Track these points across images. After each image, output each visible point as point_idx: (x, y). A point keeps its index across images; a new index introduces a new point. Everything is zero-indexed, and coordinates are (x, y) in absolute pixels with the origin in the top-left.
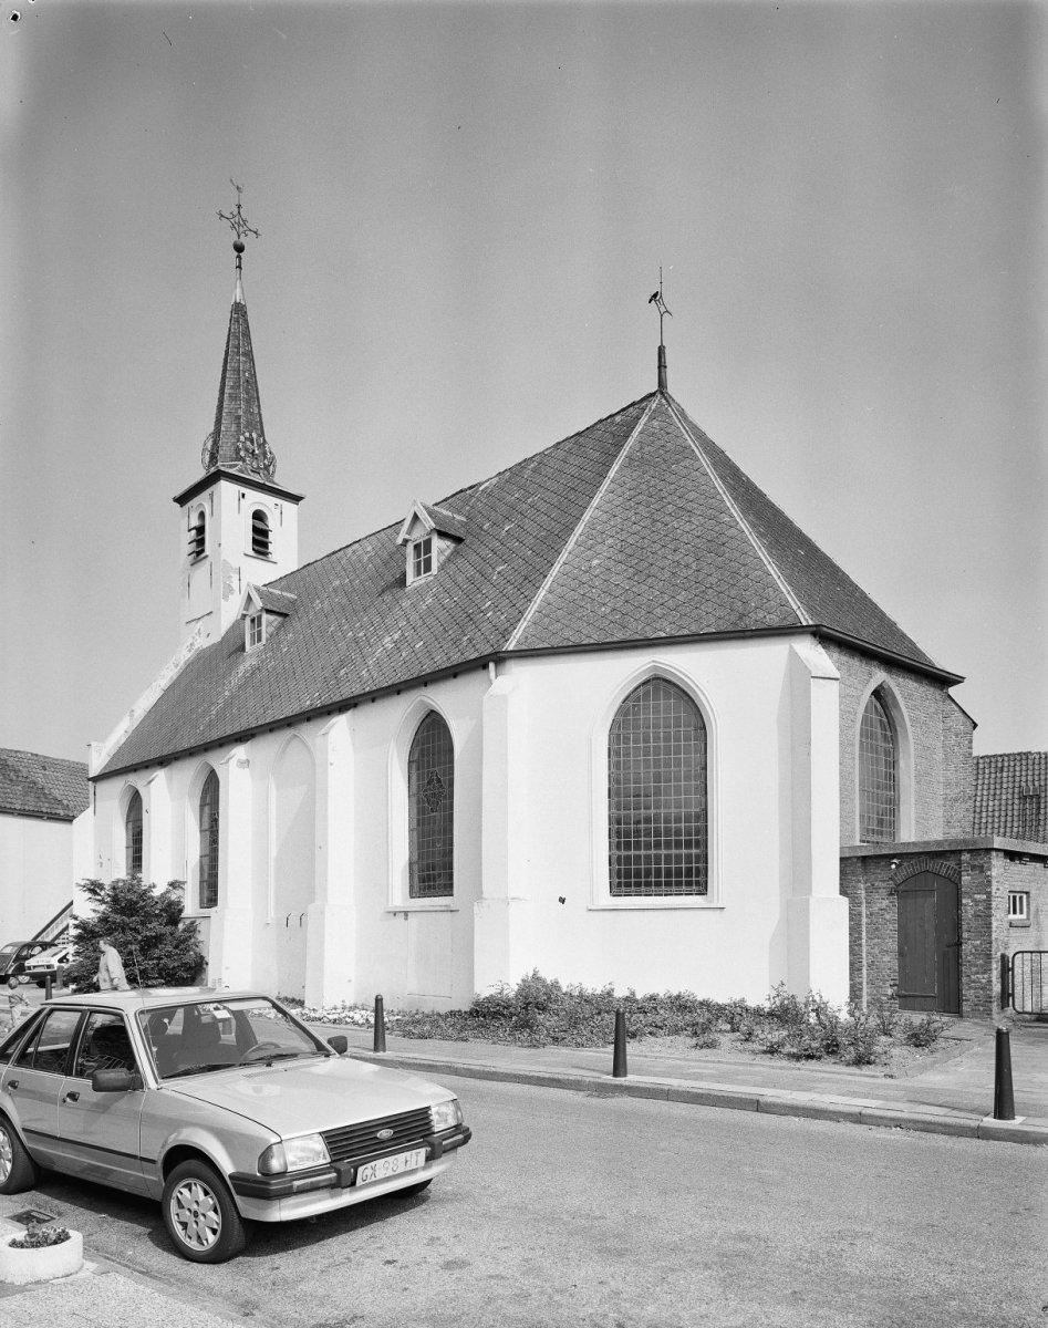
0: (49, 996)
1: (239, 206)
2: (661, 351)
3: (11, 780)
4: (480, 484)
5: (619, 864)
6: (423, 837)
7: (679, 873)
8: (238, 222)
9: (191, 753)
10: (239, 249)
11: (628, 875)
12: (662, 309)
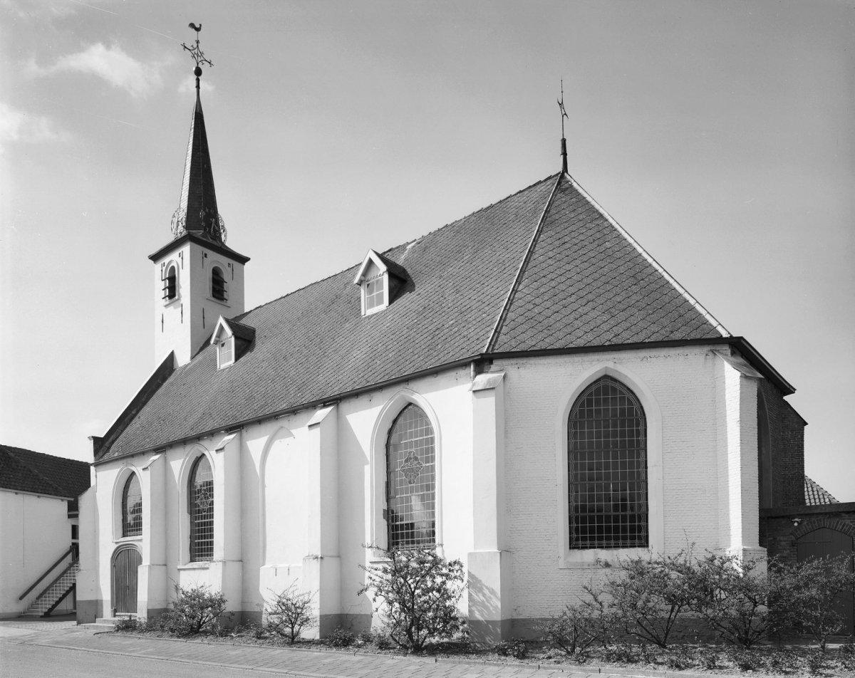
0: (444, 583)
1: (198, 42)
2: (564, 141)
3: (13, 469)
4: (408, 244)
5: (577, 523)
6: (211, 528)
7: (608, 529)
8: (196, 52)
9: (184, 442)
10: (198, 72)
11: (584, 531)
12: (564, 113)
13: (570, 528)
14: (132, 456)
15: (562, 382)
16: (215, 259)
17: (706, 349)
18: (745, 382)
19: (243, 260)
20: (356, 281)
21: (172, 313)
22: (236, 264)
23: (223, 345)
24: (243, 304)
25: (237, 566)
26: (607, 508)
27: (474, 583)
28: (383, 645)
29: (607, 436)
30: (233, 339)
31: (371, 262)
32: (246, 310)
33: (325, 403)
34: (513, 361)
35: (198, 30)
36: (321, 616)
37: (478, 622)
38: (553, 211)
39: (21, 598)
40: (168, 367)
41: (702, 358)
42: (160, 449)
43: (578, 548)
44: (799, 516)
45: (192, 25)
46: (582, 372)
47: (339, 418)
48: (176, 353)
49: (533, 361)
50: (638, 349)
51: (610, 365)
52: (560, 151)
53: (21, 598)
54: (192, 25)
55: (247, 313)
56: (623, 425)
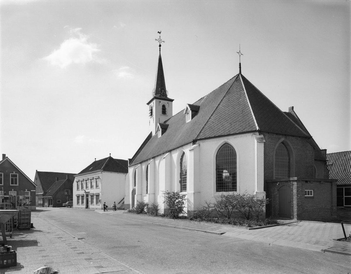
1: (160, 37)
2: (240, 64)
8: (160, 40)
10: (160, 46)
13: (217, 186)
14: (182, 146)
15: (211, 148)
16: (163, 102)
17: (252, 134)
18: (258, 143)
19: (172, 100)
20: (184, 113)
21: (152, 119)
22: (170, 102)
23: (188, 114)
24: (172, 114)
25: (153, 195)
26: (226, 182)
27: (189, 201)
28: (163, 216)
29: (226, 160)
30: (191, 111)
31: (187, 108)
32: (173, 115)
33: (167, 152)
34: (202, 141)
35: (160, 33)
36: (164, 209)
37: (189, 211)
38: (231, 89)
39: (119, 203)
40: (150, 136)
41: (251, 136)
42: (141, 163)
43: (219, 191)
44: (280, 182)
45: (158, 32)
46: (220, 142)
47: (171, 155)
48: (152, 132)
49: (207, 140)
50: (243, 134)
51: (226, 140)
52: (239, 67)
53: (119, 203)
54: (158, 32)
55: (173, 116)
56: (231, 157)
